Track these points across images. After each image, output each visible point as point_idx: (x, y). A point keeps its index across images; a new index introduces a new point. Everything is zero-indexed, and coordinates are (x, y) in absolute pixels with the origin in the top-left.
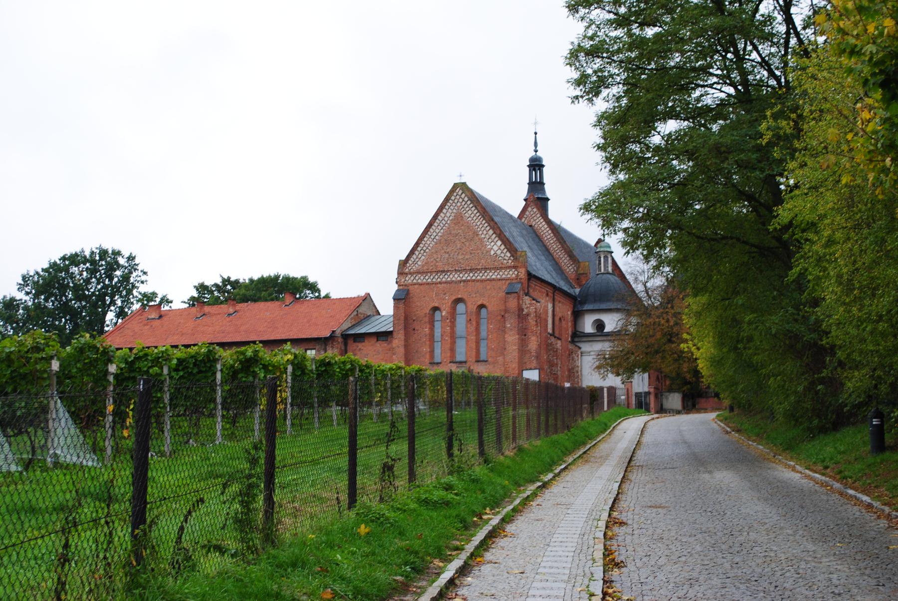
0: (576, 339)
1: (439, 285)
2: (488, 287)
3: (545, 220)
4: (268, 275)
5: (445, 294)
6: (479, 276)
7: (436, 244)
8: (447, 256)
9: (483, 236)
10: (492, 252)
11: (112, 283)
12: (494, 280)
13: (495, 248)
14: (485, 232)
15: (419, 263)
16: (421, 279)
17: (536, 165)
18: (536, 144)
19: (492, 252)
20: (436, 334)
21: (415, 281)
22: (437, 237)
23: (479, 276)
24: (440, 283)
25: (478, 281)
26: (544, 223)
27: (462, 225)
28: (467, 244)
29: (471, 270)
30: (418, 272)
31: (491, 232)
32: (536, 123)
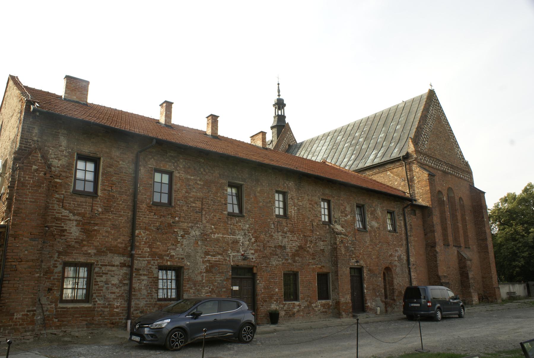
17: (280, 104)
18: (279, 91)
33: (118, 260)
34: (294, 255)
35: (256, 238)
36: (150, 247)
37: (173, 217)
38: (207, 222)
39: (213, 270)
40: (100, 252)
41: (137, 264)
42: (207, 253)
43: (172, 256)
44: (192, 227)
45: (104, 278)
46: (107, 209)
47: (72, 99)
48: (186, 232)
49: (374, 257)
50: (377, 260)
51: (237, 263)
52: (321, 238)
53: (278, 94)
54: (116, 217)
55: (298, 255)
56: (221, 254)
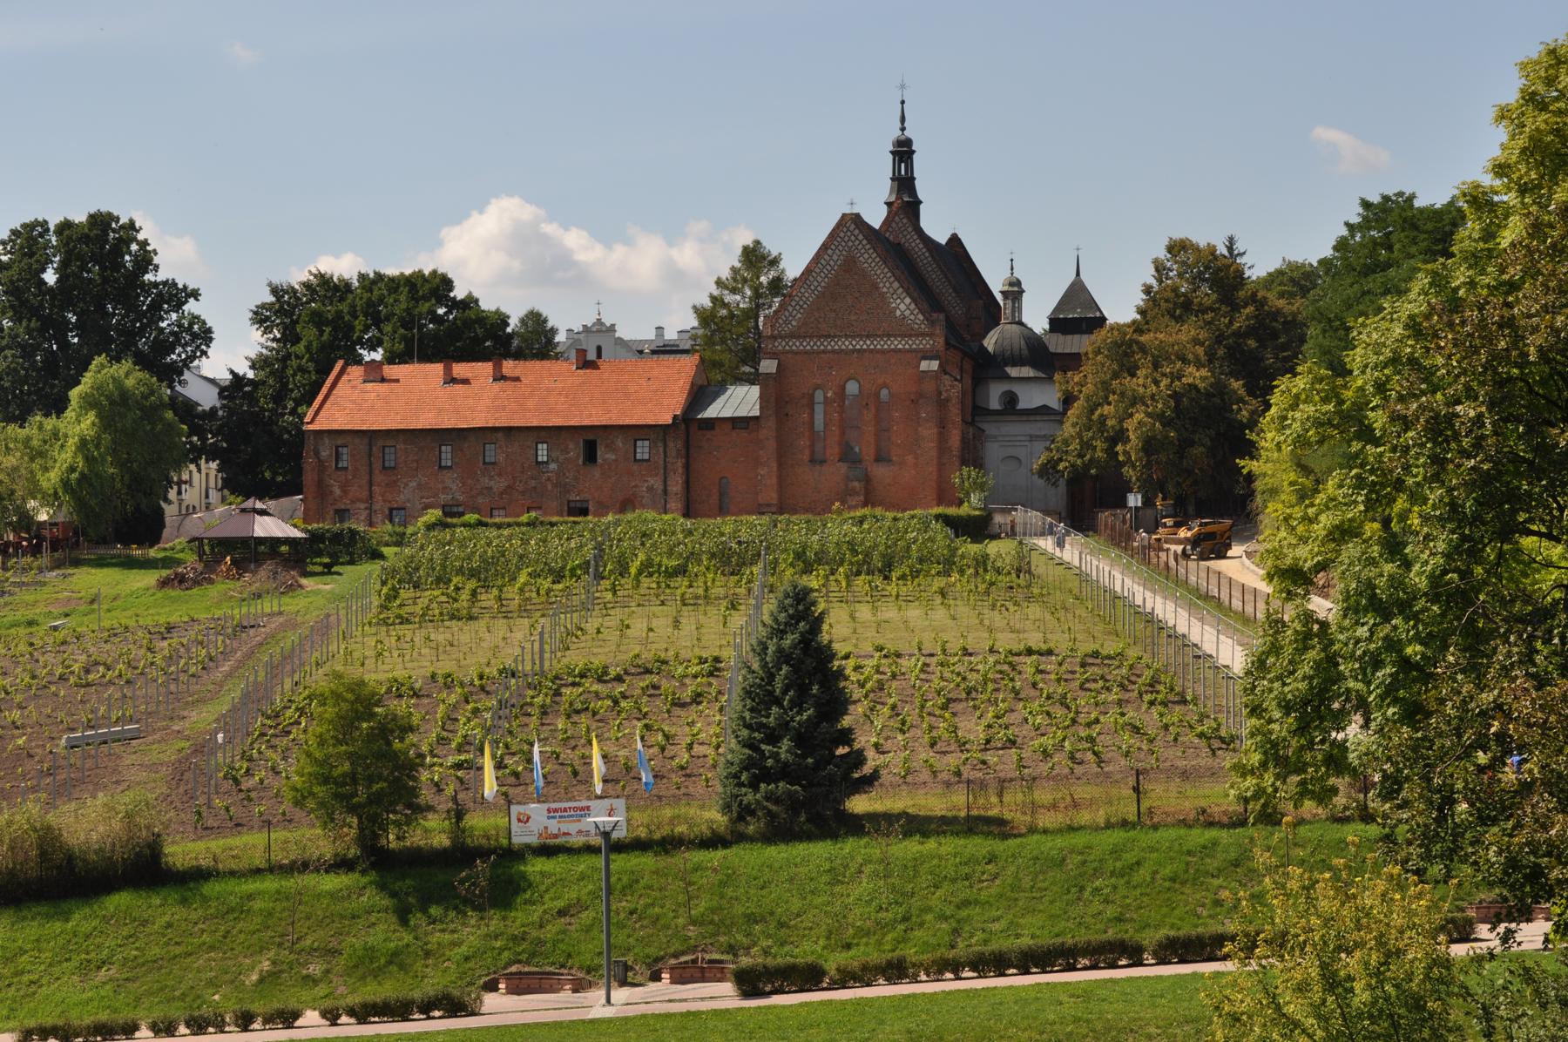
0: (977, 418)
2: (893, 361)
4: (493, 309)
5: (831, 368)
6: (880, 344)
8: (833, 315)
9: (885, 290)
10: (898, 313)
13: (902, 307)
17: (903, 152)
18: (903, 119)
20: (816, 422)
23: (880, 344)
24: (824, 352)
25: (878, 351)
29: (868, 337)
30: (792, 336)
31: (896, 285)
32: (903, 87)
33: (363, 506)
35: (464, 484)
40: (353, 502)
41: (374, 507)
46: (354, 477)
48: (407, 485)
54: (1547, 641)
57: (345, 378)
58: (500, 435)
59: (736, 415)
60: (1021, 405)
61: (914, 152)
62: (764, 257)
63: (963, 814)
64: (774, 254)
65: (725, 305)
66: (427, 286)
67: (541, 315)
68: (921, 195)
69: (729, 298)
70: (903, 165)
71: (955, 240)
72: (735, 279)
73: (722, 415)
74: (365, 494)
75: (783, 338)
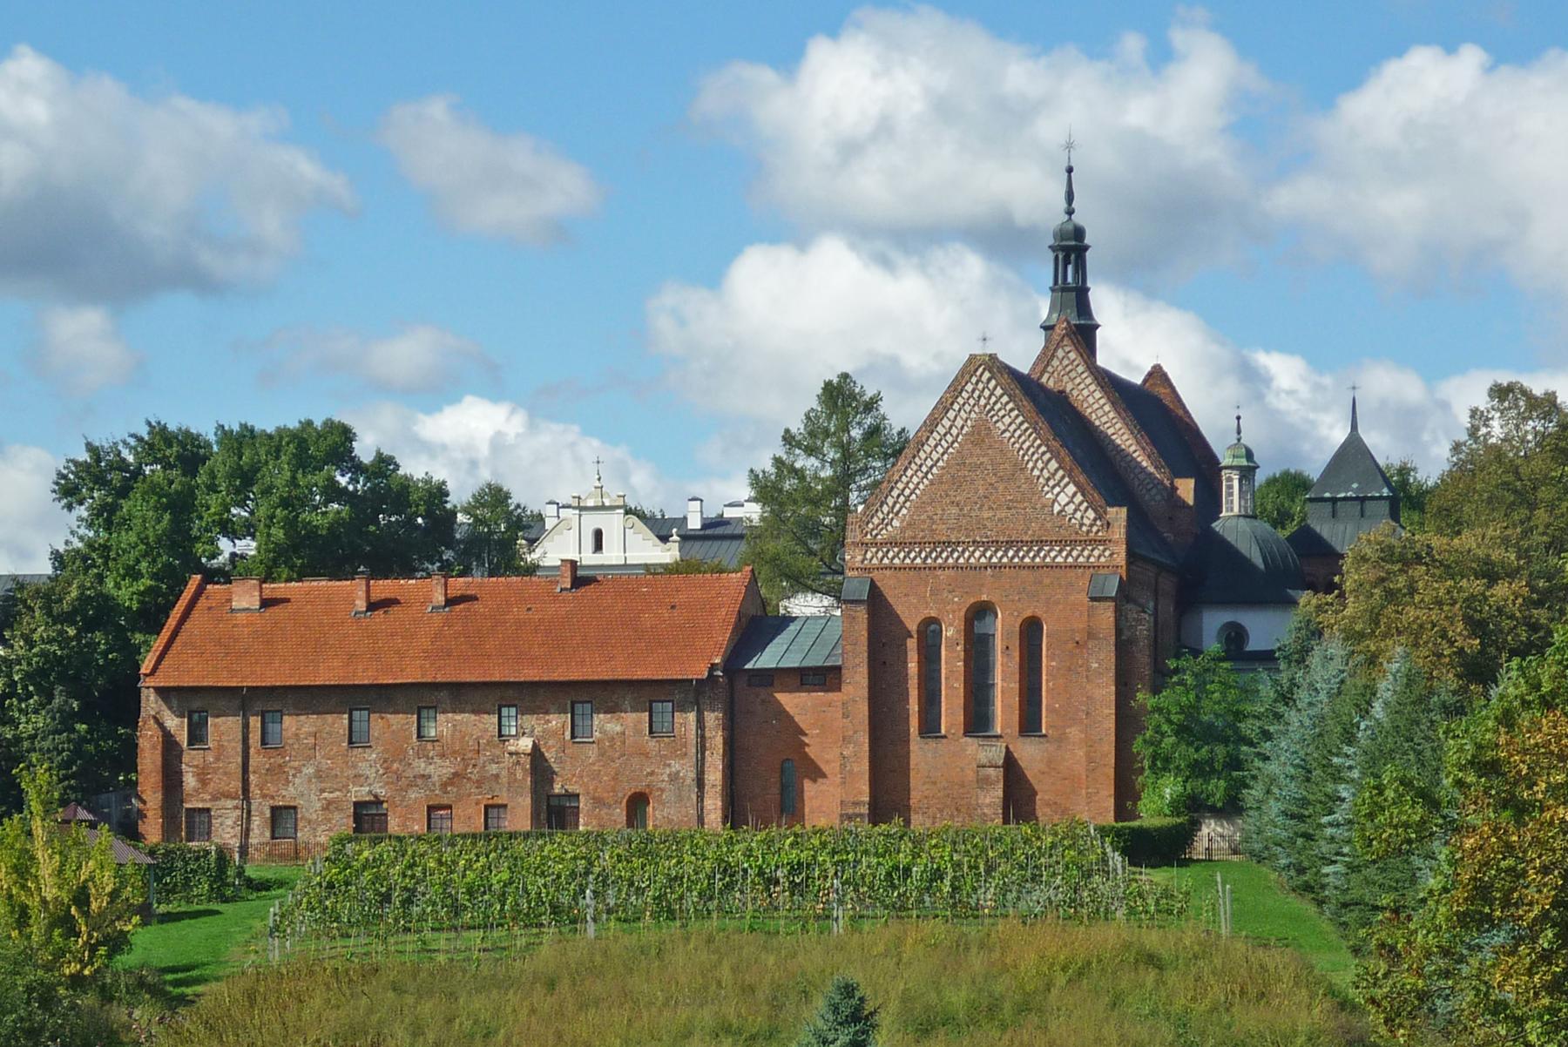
1: (939, 572)
3: (1088, 368)
7: (932, 483)
8: (955, 510)
10: (1057, 508)
11: (99, 653)
12: (1058, 566)
13: (1063, 499)
14: (1040, 465)
15: (896, 523)
16: (897, 557)
18: (1070, 197)
19: (1057, 508)
21: (886, 561)
22: (935, 470)
26: (1092, 387)
27: (990, 447)
28: (1001, 487)
29: (1010, 544)
31: (1053, 465)
34: (444, 786)
36: (261, 789)
37: (284, 757)
38: (323, 758)
39: (331, 807)
40: (215, 798)
42: (322, 791)
43: (284, 796)
44: (304, 765)
45: (219, 821)
46: (217, 759)
47: (241, 607)
49: (605, 778)
50: (612, 783)
51: (360, 799)
52: (493, 760)
53: (1064, 205)
55: (452, 784)
56: (340, 790)
57: (202, 603)
58: (443, 694)
59: (805, 664)
60: (1253, 645)
61: (1086, 248)
62: (853, 396)
63: (138, 734)
64: (870, 393)
65: (799, 474)
66: (323, 445)
67: (501, 490)
68: (1098, 317)
69: (804, 462)
70: (1070, 269)
71: (1157, 374)
72: (812, 434)
73: (784, 664)
74: (236, 785)
75: (878, 545)
